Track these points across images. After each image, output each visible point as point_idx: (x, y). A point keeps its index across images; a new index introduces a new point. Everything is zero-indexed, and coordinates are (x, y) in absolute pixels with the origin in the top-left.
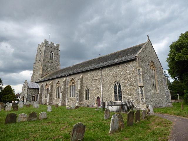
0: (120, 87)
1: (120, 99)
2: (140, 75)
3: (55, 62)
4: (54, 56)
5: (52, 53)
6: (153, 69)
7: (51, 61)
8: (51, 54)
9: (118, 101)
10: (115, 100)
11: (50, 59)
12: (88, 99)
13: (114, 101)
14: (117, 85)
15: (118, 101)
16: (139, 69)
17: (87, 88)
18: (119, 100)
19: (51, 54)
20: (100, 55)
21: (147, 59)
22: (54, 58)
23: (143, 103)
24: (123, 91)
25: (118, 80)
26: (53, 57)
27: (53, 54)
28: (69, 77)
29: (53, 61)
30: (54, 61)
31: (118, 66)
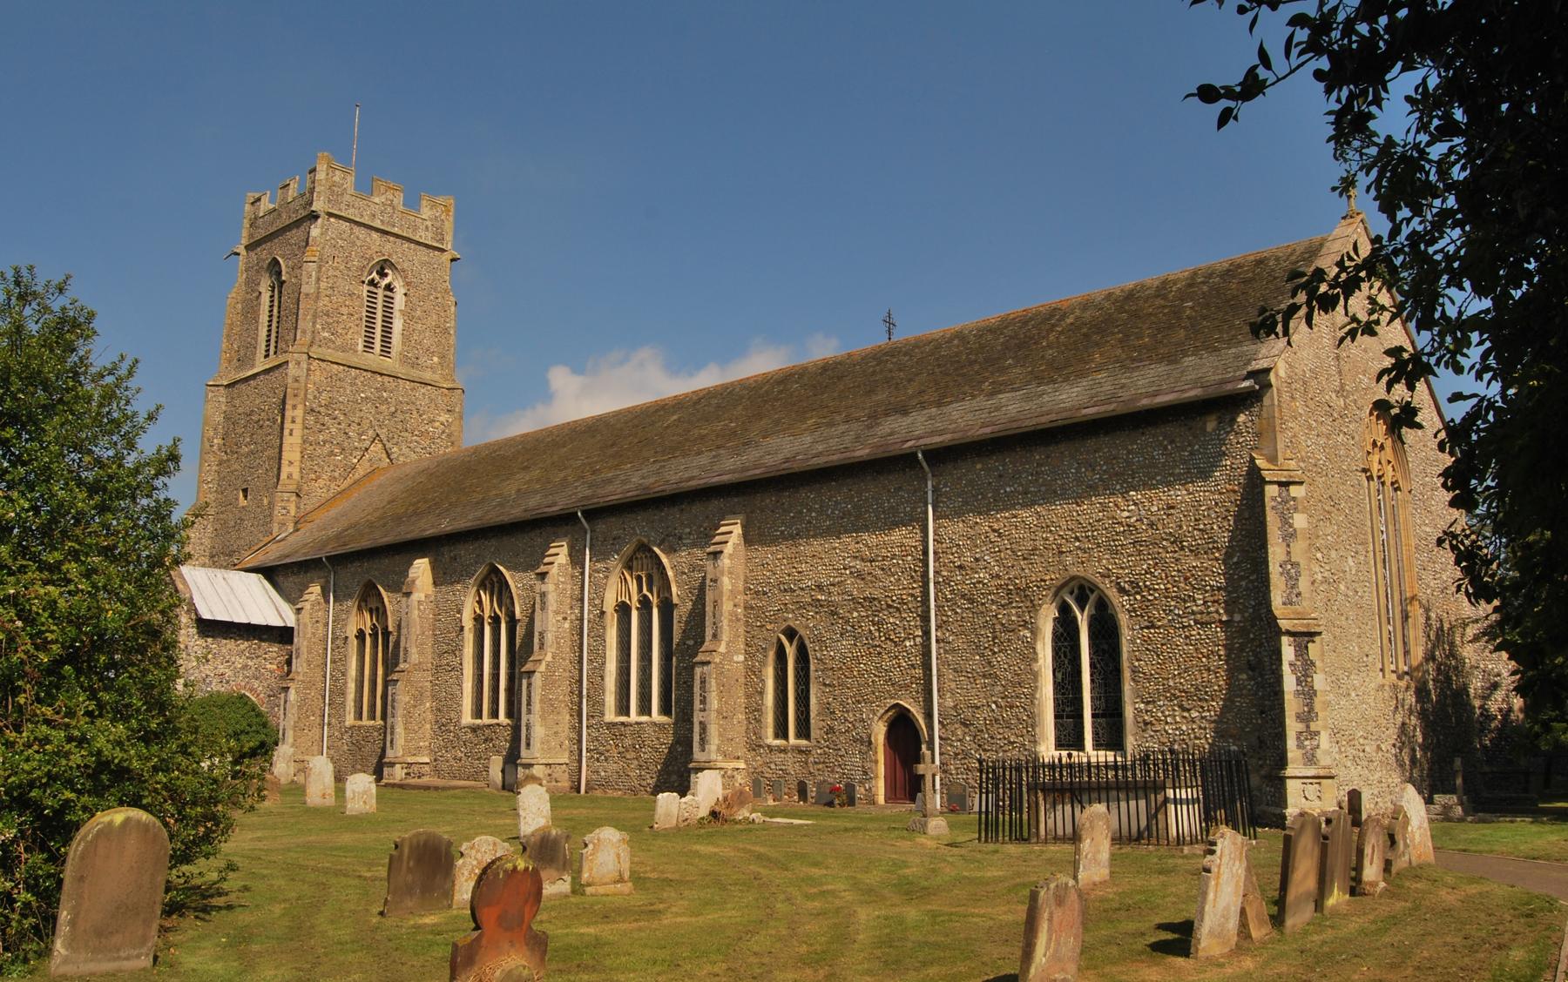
0: (1105, 631)
1: (1111, 737)
2: (1293, 535)
3: (415, 374)
4: (408, 315)
5: (389, 288)
6: (1388, 479)
7: (374, 359)
8: (380, 292)
9: (1091, 753)
10: (777, 736)
11: (369, 345)
12: (804, 730)
13: (1048, 751)
14: (791, 651)
15: (1091, 753)
16: (1280, 484)
17: (791, 633)
18: (1098, 745)
19: (380, 292)
20: (889, 323)
21: (1340, 391)
22: (406, 337)
23: (1311, 772)
24: (1134, 671)
25: (1092, 571)
26: (398, 325)
27: (399, 301)
28: (601, 526)
29: (389, 364)
30: (404, 359)
31: (1091, 443)
